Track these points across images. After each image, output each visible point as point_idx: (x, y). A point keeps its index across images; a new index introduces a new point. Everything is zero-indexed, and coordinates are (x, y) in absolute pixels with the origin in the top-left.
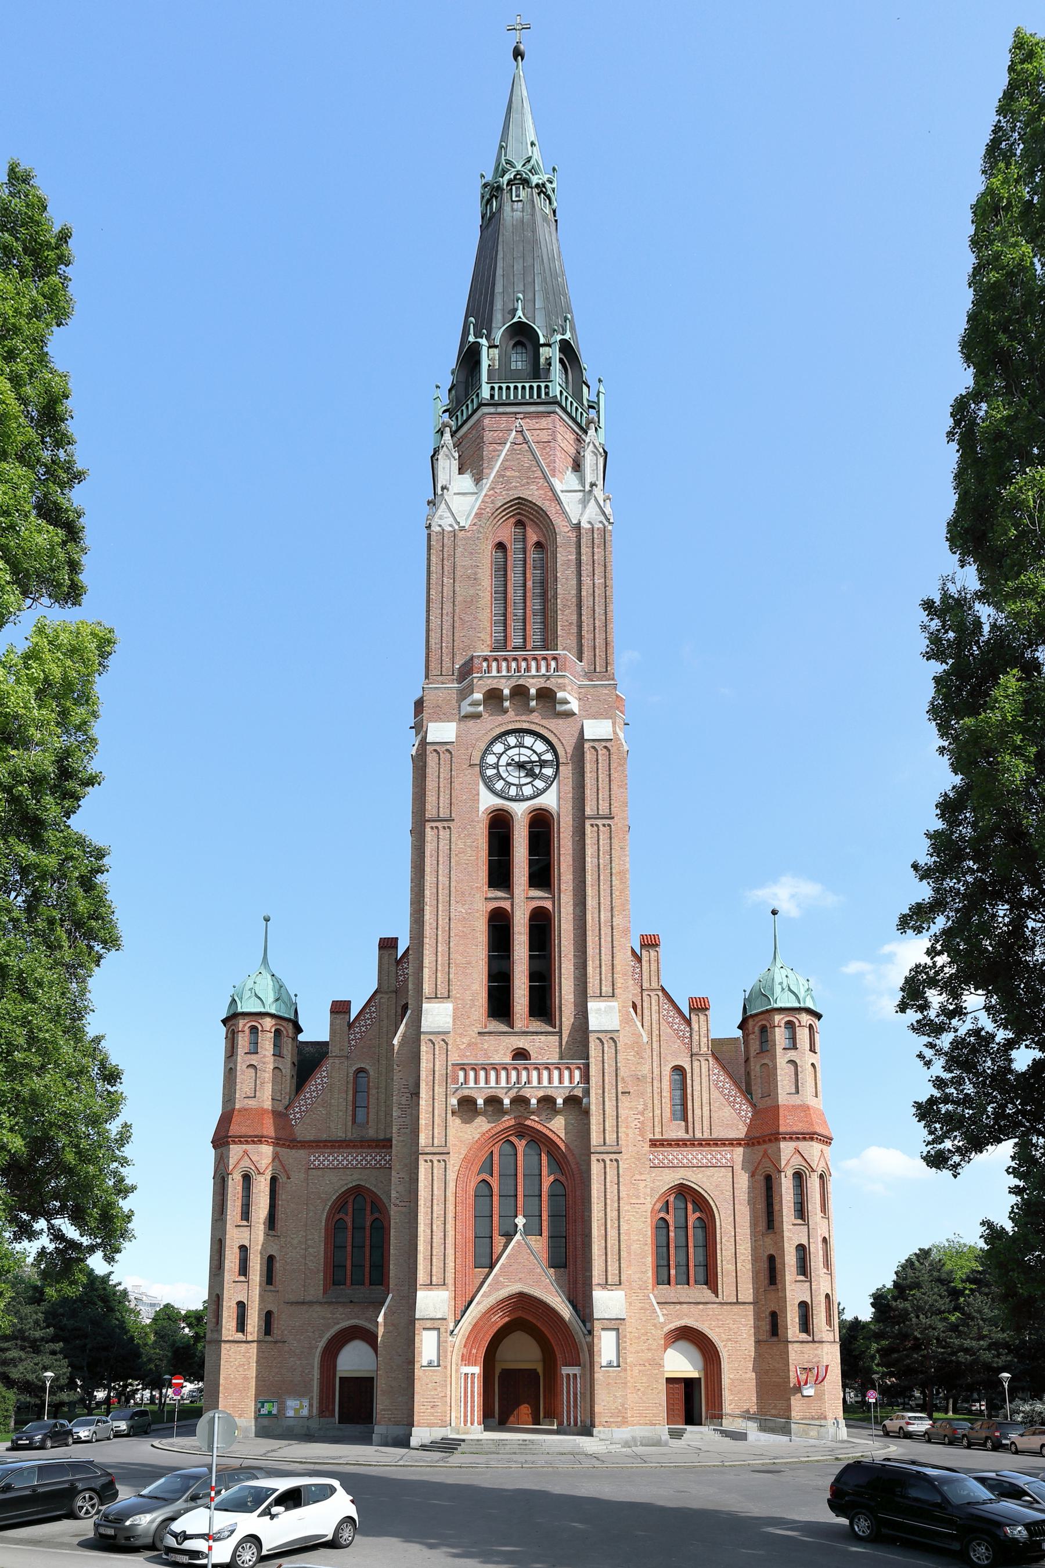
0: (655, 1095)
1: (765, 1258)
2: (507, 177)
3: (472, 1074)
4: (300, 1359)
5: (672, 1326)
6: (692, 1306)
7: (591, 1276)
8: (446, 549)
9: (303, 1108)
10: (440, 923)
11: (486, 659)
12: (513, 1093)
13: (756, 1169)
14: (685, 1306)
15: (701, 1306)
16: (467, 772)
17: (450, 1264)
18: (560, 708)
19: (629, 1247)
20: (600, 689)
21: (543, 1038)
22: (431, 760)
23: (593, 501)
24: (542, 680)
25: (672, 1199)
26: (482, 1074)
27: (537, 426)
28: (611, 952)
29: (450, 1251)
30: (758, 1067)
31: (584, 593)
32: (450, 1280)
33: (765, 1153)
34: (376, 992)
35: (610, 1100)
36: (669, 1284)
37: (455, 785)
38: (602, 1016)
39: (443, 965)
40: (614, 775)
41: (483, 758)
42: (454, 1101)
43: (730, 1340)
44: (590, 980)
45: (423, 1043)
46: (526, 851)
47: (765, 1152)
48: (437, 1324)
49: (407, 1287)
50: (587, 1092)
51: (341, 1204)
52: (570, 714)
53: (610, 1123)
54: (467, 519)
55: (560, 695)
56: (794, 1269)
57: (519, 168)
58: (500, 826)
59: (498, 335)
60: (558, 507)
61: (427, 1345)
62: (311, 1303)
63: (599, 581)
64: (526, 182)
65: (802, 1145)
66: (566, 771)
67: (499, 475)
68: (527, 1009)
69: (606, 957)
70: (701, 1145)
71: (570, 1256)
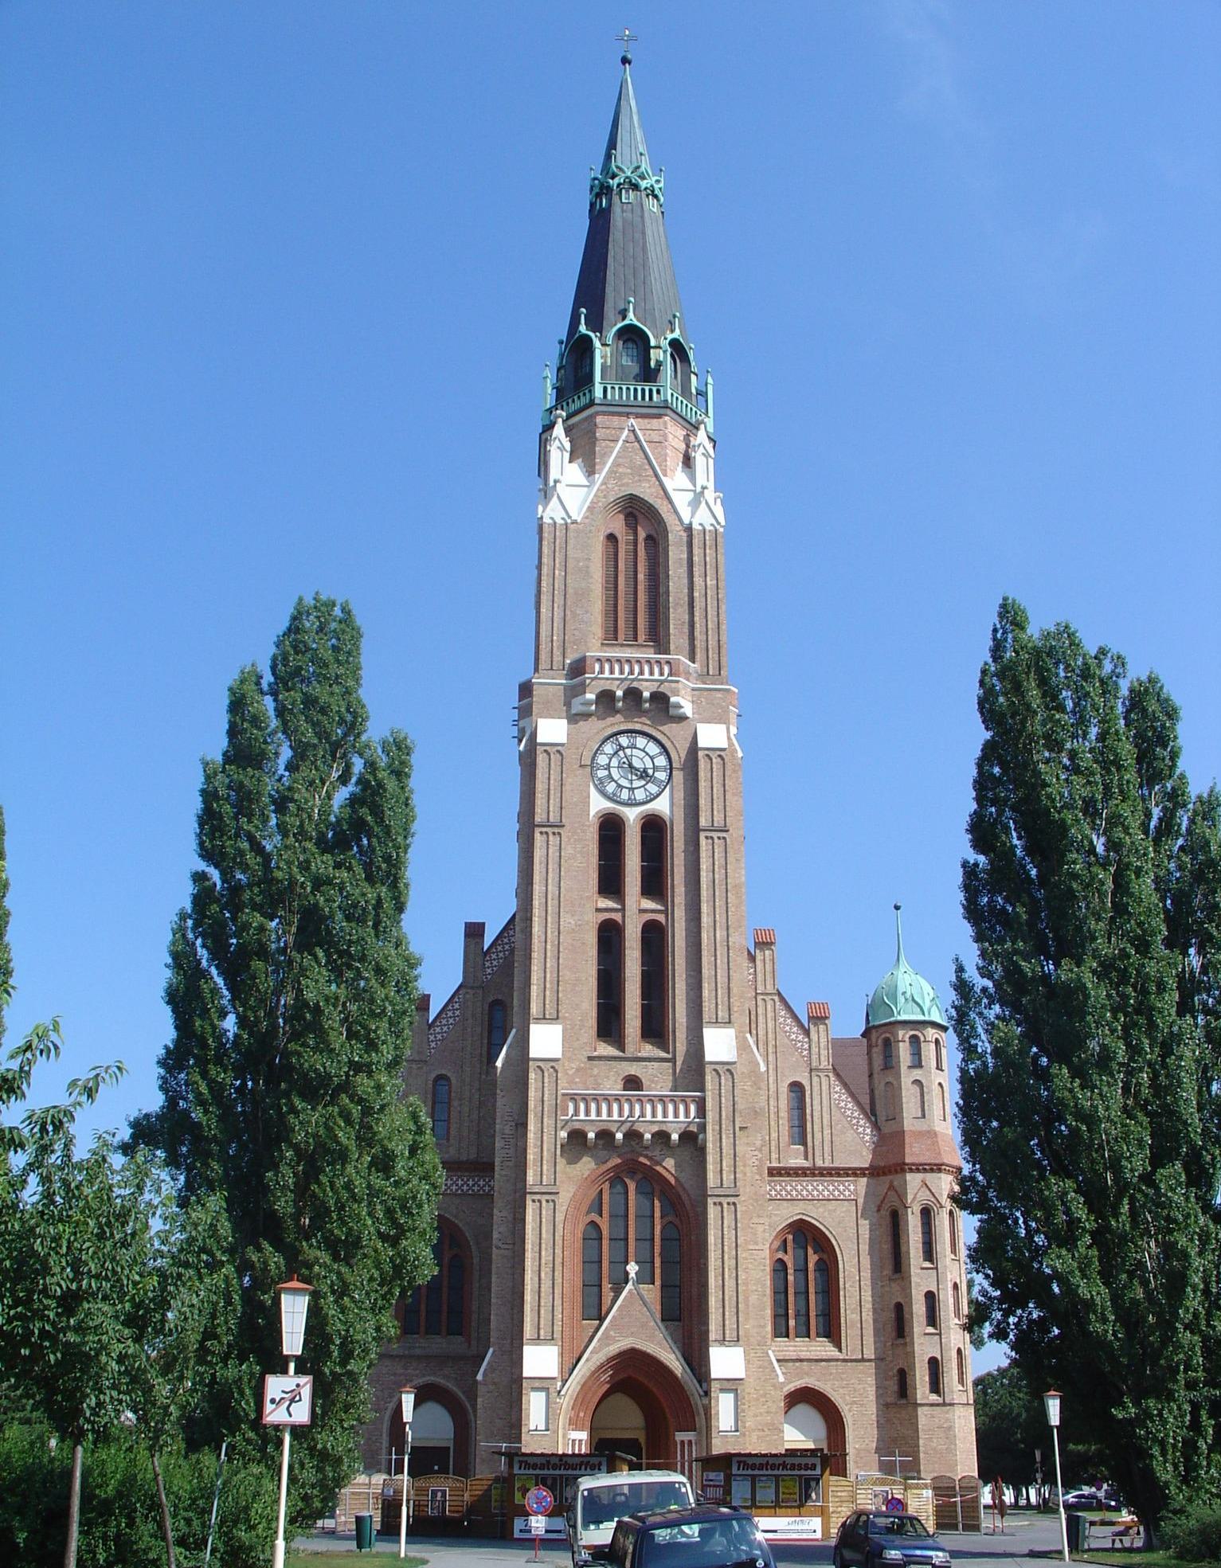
1: (892, 1306)
2: (616, 181)
5: (791, 1387)
7: (707, 1331)
12: (625, 1128)
19: (747, 1299)
22: (541, 759)
23: (703, 504)
24: (656, 684)
25: (790, 1237)
28: (726, 969)
29: (558, 1302)
31: (696, 594)
33: (891, 1187)
36: (787, 1336)
38: (719, 1044)
41: (593, 759)
42: (563, 1134)
44: (705, 1004)
46: (642, 857)
48: (545, 1384)
50: (703, 1127)
52: (683, 718)
55: (673, 699)
56: (923, 1320)
58: (611, 829)
63: (711, 582)
65: (930, 1177)
66: (678, 776)
67: (611, 471)
68: (639, 1032)
70: (822, 1175)
71: (686, 1311)
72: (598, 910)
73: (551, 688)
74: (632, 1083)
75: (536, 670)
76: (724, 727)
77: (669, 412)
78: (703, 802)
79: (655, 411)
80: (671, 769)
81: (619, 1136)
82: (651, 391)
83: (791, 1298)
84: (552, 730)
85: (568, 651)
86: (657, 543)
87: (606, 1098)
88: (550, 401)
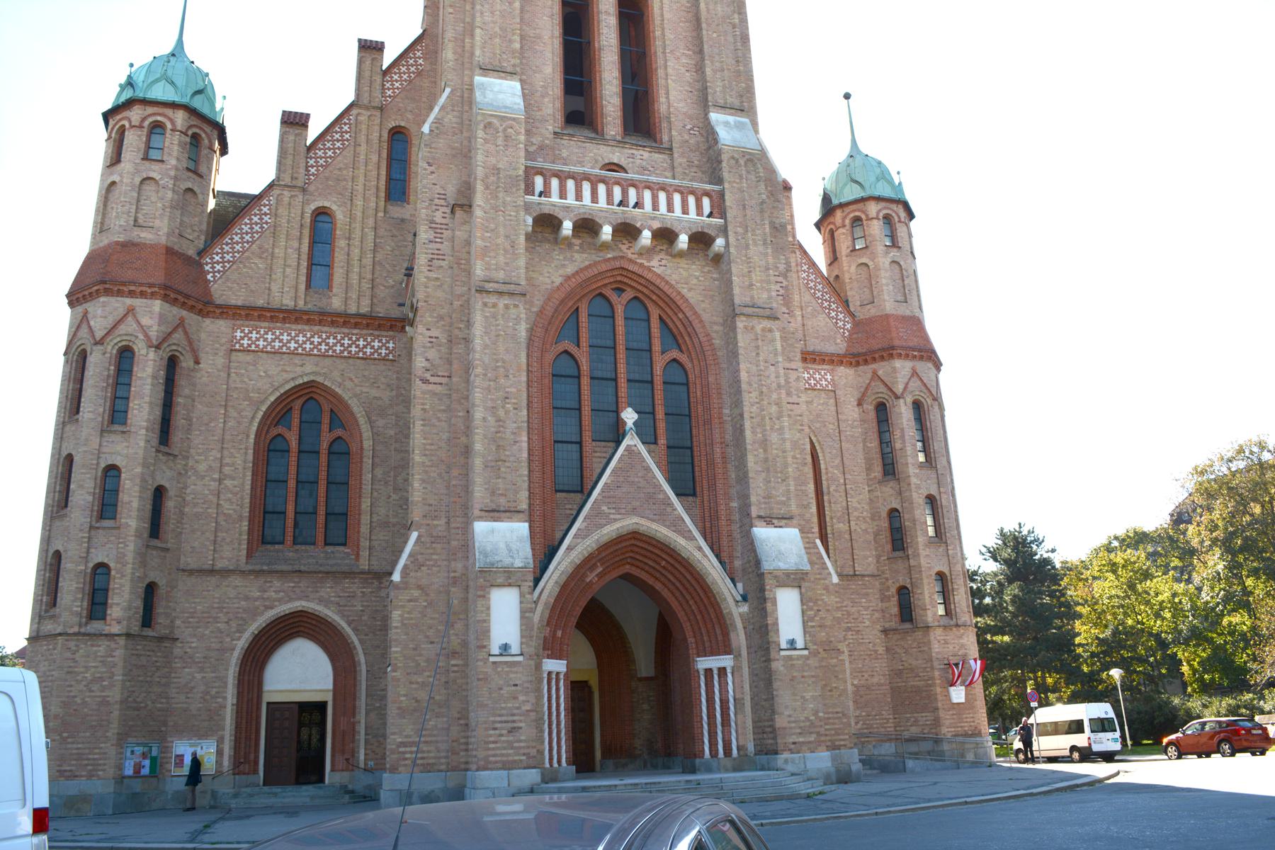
4: (202, 670)
9: (228, 257)
13: (864, 394)
30: (853, 268)
34: (271, 186)
43: (849, 629)
47: (875, 373)
49: (443, 521)
51: (280, 412)
62: (225, 573)
87: (587, 177)
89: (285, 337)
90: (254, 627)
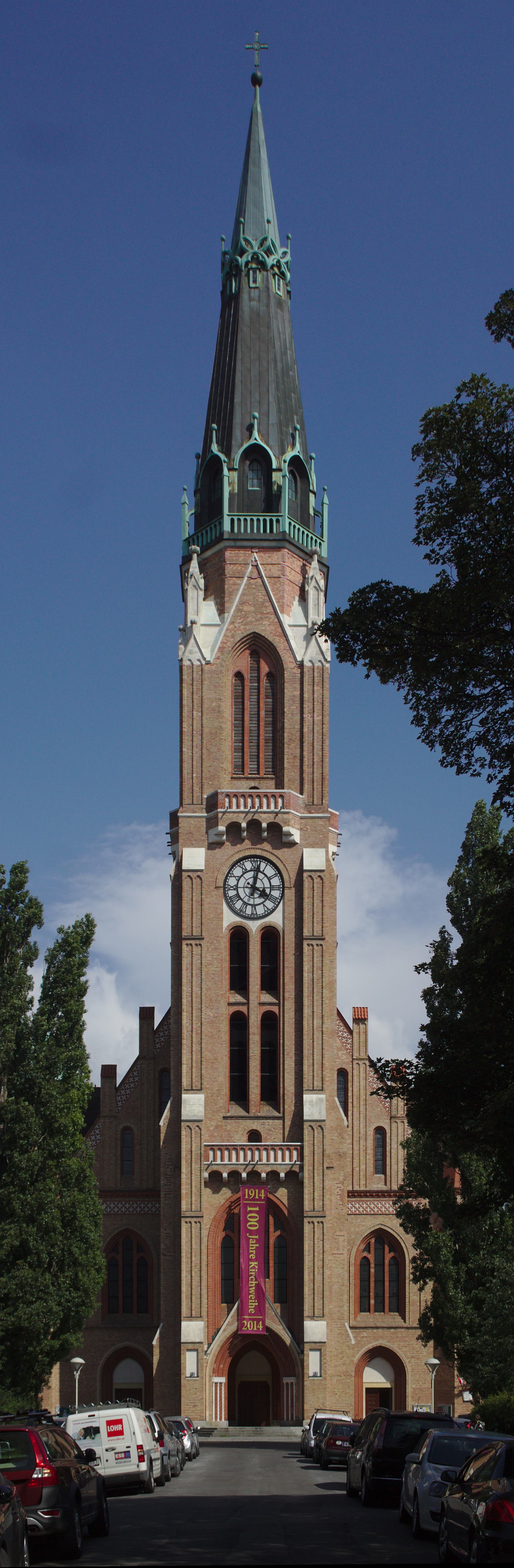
0: (362, 1153)
3: (219, 1153)
6: (386, 1330)
8: (195, 683)
10: (194, 1026)
11: (228, 795)
12: (249, 1168)
14: (380, 1330)
15: (392, 1330)
16: (213, 893)
17: (205, 1301)
18: (284, 839)
19: (331, 1288)
20: (317, 821)
21: (271, 1121)
22: (186, 884)
25: (373, 1240)
26: (226, 1153)
27: (269, 561)
29: (204, 1291)
31: (305, 730)
32: (204, 1314)
35: (318, 1175)
36: (369, 1311)
37: (205, 906)
38: (315, 1106)
39: (196, 1062)
40: (326, 898)
41: (225, 881)
43: (413, 1357)
44: (305, 1076)
45: (183, 1129)
48: (196, 1346)
50: (302, 1168)
52: (293, 844)
53: (317, 1194)
54: (212, 651)
55: (285, 829)
57: (256, 249)
58: (239, 936)
59: (237, 455)
60: (286, 643)
61: (189, 1362)
63: (317, 718)
64: (262, 265)
66: (290, 894)
67: (238, 610)
68: (259, 1097)
69: (317, 1057)
72: (230, 1004)
73: (192, 821)
74: (254, 1136)
75: (181, 804)
76: (324, 850)
77: (287, 545)
78: (306, 916)
79: (273, 544)
80: (283, 888)
81: (244, 1175)
82: (271, 521)
83: (372, 1285)
84: (194, 857)
85: (205, 786)
86: (276, 677)
88: (187, 531)
89: (112, 1206)
90: (107, 1354)
